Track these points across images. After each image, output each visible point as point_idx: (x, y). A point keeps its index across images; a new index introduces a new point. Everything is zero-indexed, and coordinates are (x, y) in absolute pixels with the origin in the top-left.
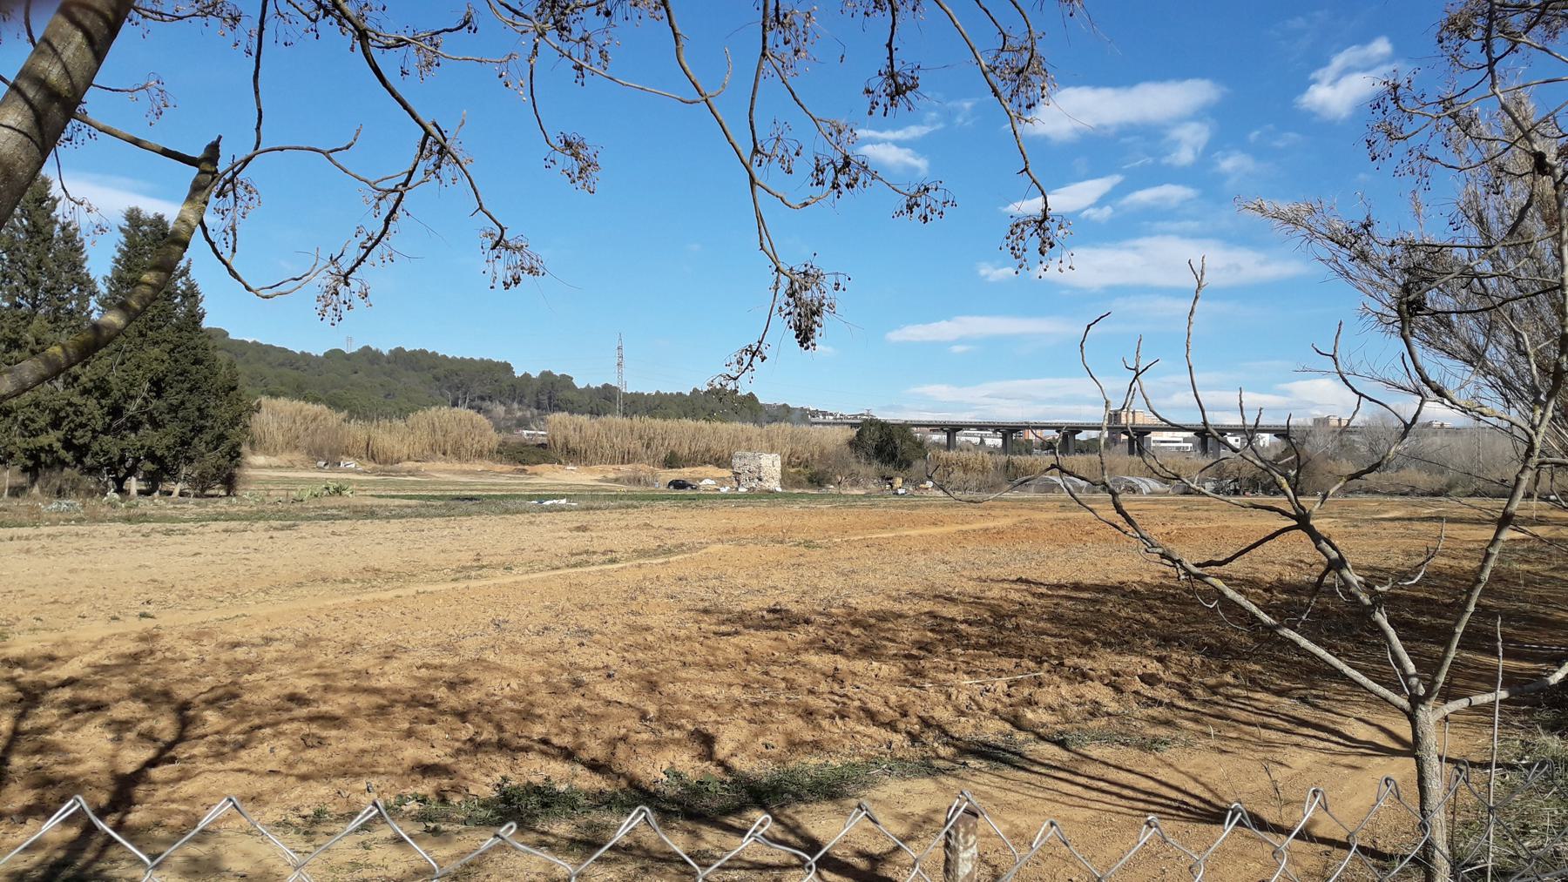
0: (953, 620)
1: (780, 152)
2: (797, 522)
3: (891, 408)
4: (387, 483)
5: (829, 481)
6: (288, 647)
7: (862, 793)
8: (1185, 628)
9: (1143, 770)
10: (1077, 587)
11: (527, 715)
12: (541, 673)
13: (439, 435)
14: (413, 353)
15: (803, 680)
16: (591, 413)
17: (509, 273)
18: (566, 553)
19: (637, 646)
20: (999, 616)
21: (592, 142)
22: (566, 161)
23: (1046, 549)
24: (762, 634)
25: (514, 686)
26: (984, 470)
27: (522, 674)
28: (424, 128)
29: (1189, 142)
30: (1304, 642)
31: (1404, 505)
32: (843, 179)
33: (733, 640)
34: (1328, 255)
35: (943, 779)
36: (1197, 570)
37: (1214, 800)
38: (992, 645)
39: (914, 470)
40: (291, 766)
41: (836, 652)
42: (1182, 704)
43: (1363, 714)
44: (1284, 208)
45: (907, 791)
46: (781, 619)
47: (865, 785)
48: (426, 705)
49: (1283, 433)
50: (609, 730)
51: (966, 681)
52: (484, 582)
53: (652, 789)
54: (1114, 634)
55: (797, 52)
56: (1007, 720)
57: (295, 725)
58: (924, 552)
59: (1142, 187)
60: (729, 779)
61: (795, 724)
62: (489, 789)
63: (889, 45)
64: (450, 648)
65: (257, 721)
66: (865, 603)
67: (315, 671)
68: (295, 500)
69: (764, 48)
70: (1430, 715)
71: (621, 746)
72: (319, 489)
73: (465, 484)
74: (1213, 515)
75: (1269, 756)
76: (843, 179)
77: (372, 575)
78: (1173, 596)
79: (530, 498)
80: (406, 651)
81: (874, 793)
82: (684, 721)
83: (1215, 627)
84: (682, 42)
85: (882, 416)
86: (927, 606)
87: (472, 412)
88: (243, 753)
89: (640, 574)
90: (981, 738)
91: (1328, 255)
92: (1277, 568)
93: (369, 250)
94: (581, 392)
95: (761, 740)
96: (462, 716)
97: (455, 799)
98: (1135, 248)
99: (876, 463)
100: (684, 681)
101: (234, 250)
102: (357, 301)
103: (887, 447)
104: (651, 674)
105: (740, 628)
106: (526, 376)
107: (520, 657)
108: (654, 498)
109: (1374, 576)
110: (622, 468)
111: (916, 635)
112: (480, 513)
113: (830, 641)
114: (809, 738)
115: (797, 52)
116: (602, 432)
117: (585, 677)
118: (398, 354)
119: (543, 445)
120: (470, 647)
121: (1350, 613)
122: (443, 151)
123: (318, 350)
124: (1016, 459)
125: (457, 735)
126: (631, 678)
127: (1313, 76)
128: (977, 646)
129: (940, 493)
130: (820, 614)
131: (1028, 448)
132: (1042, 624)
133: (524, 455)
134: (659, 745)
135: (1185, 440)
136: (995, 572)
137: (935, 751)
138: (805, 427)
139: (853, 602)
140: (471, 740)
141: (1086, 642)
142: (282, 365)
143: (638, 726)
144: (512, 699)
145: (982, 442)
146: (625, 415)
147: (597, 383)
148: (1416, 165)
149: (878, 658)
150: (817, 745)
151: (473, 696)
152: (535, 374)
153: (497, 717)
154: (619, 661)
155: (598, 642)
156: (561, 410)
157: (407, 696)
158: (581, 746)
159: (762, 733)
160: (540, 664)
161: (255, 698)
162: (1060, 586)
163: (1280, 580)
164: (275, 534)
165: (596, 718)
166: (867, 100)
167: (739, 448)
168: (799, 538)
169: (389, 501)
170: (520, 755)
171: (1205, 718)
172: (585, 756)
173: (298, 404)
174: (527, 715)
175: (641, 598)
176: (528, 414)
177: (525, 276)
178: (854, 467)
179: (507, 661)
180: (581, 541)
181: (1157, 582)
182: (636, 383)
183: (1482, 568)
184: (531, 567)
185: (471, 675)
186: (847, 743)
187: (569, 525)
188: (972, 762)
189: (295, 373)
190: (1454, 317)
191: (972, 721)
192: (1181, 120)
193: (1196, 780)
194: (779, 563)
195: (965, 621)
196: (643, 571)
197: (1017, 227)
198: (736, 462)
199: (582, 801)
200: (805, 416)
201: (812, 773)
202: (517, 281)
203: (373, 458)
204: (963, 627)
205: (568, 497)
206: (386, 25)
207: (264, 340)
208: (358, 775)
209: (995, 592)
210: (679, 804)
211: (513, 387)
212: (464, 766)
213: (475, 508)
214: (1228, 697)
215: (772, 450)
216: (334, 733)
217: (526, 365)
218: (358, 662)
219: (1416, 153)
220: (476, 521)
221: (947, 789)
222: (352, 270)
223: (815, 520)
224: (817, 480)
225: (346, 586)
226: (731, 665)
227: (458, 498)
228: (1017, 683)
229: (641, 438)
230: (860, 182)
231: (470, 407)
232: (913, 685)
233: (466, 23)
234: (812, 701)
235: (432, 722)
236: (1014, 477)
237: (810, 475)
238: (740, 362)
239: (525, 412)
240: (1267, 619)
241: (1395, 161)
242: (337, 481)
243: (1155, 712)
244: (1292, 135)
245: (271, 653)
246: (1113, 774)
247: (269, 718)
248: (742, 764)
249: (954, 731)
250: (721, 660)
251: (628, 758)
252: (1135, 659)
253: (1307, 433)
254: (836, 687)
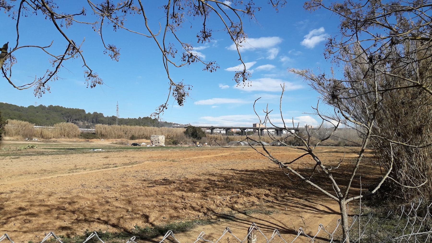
0: (214, 181)
1: (171, 52)
2: (170, 155)
3: (196, 123)
4: (47, 145)
5: (179, 143)
6: (18, 193)
7: (191, 230)
8: (275, 181)
9: (266, 220)
10: (247, 171)
11: (93, 212)
12: (96, 199)
13: (63, 131)
14: (55, 107)
15: (174, 199)
16: (109, 124)
17: (93, 83)
18: (102, 164)
19: (124, 191)
20: (227, 179)
21: (118, 47)
22: (110, 52)
23: (238, 161)
24: (161, 186)
25: (89, 203)
26: (221, 139)
27: (91, 200)
28: (69, 42)
29: (273, 53)
30: (312, 184)
31: (327, 148)
32: (191, 60)
33: (153, 188)
34: (311, 84)
35: (213, 225)
36: (285, 165)
37: (285, 227)
38: (225, 187)
39: (202, 140)
40: (21, 229)
41: (182, 191)
42: (275, 201)
43: (321, 203)
44: (300, 71)
45: (204, 229)
46: (166, 182)
47: (192, 228)
48: (62, 209)
49: (297, 130)
50: (117, 215)
51: (219, 197)
52: (77, 173)
53: (131, 231)
54: (257, 183)
55: (179, 25)
56: (230, 208)
57: (21, 217)
58: (206, 162)
59: (261, 65)
60: (153, 228)
61: (172, 211)
62: (82, 233)
63: (204, 24)
64: (69, 193)
65: (9, 216)
66: (190, 177)
67: (27, 200)
68: (19, 150)
69: (167, 23)
70: (344, 202)
71: (121, 220)
72: (26, 147)
73: (71, 145)
74: (280, 151)
75: (298, 215)
76: (191, 60)
77: (44, 172)
78: (272, 173)
79: (91, 149)
80: (55, 193)
81: (194, 230)
82: (139, 212)
83: (283, 181)
84: (147, 20)
85: (193, 125)
86: (207, 177)
87: (73, 124)
88: (5, 226)
89: (124, 170)
90: (223, 213)
91: (311, 84)
92: (297, 165)
93: (51, 76)
94: (106, 118)
95: (162, 216)
96: (74, 212)
97: (72, 237)
98: (260, 81)
99: (192, 138)
100: (139, 200)
101: (10, 76)
102: (46, 91)
103: (195, 133)
104: (129, 199)
105: (155, 185)
106: (89, 113)
107: (90, 195)
108: (128, 148)
109: (328, 167)
110: (118, 140)
111: (204, 185)
112: (75, 153)
113: (181, 188)
114: (176, 215)
115: (179, 25)
116: (112, 130)
117: (109, 200)
118: (51, 107)
119: (94, 134)
120: (74, 192)
121: (316, 177)
122: (74, 48)
123: (26, 106)
124: (229, 136)
125: (72, 218)
126: (123, 200)
127: (305, 37)
128: (221, 188)
129: (209, 146)
130: (178, 180)
131: (232, 134)
132: (238, 181)
133: (88, 136)
134: (133, 219)
135: (273, 132)
136: (225, 167)
137: (211, 217)
138: (171, 128)
139: (187, 176)
140: (76, 219)
141: (250, 186)
142: (15, 110)
143: (126, 214)
144: (88, 207)
145: (220, 132)
146: (119, 124)
147: (110, 116)
148: (336, 60)
149: (194, 192)
150: (178, 217)
151: (76, 206)
152: (92, 113)
153: (84, 212)
154: (119, 195)
155: (113, 190)
156: (100, 123)
157: (56, 207)
158: (110, 220)
159: (162, 214)
160: (96, 197)
161: (8, 209)
162: (242, 171)
163: (298, 168)
164: (13, 160)
165: (113, 212)
166: (197, 39)
167: (153, 134)
168: (170, 159)
169: (48, 150)
170: (91, 223)
171: (282, 205)
172: (111, 223)
173: (19, 122)
174: (93, 212)
175: (125, 177)
176: (90, 124)
177: (97, 85)
178: (186, 139)
179: (86, 196)
180: (106, 161)
181: (267, 169)
182: (122, 115)
183: (357, 164)
184: (91, 169)
185: (75, 200)
186: (187, 216)
187: (102, 156)
188: (221, 220)
189: (18, 112)
190: (342, 100)
191: (221, 208)
192: (271, 47)
193: (280, 222)
194: (165, 166)
195: (218, 181)
196: (125, 169)
197: (237, 75)
198: (152, 138)
199: (110, 236)
200: (170, 125)
201: (177, 225)
202: (95, 86)
203: (43, 137)
204: (217, 182)
205: (102, 149)
206: (58, 12)
207: (9, 103)
208: (42, 231)
209: (225, 173)
210: (139, 235)
211: (85, 117)
212: (75, 227)
213: (74, 152)
214: (287, 200)
215: (162, 134)
216: (34, 218)
217: (89, 110)
218: (41, 197)
219: (336, 57)
220: (74, 156)
221: (214, 228)
222: (45, 82)
223: (175, 154)
224: (175, 143)
225: (36, 175)
226: (152, 195)
227: (69, 149)
228: (232, 197)
229: (123, 131)
230: (195, 61)
231: (72, 122)
232: (204, 199)
233: (83, 12)
234: (176, 205)
235: (64, 214)
236: (228, 141)
237: (173, 141)
238: (160, 109)
239: (89, 125)
240: (303, 178)
241: (331, 59)
242: (32, 144)
243: (268, 204)
244: (300, 52)
245: (13, 195)
246: (259, 221)
247: (13, 215)
248: (157, 223)
249: (216, 211)
250: (150, 194)
251: (123, 223)
252: (263, 190)
253: (303, 130)
254: (183, 201)
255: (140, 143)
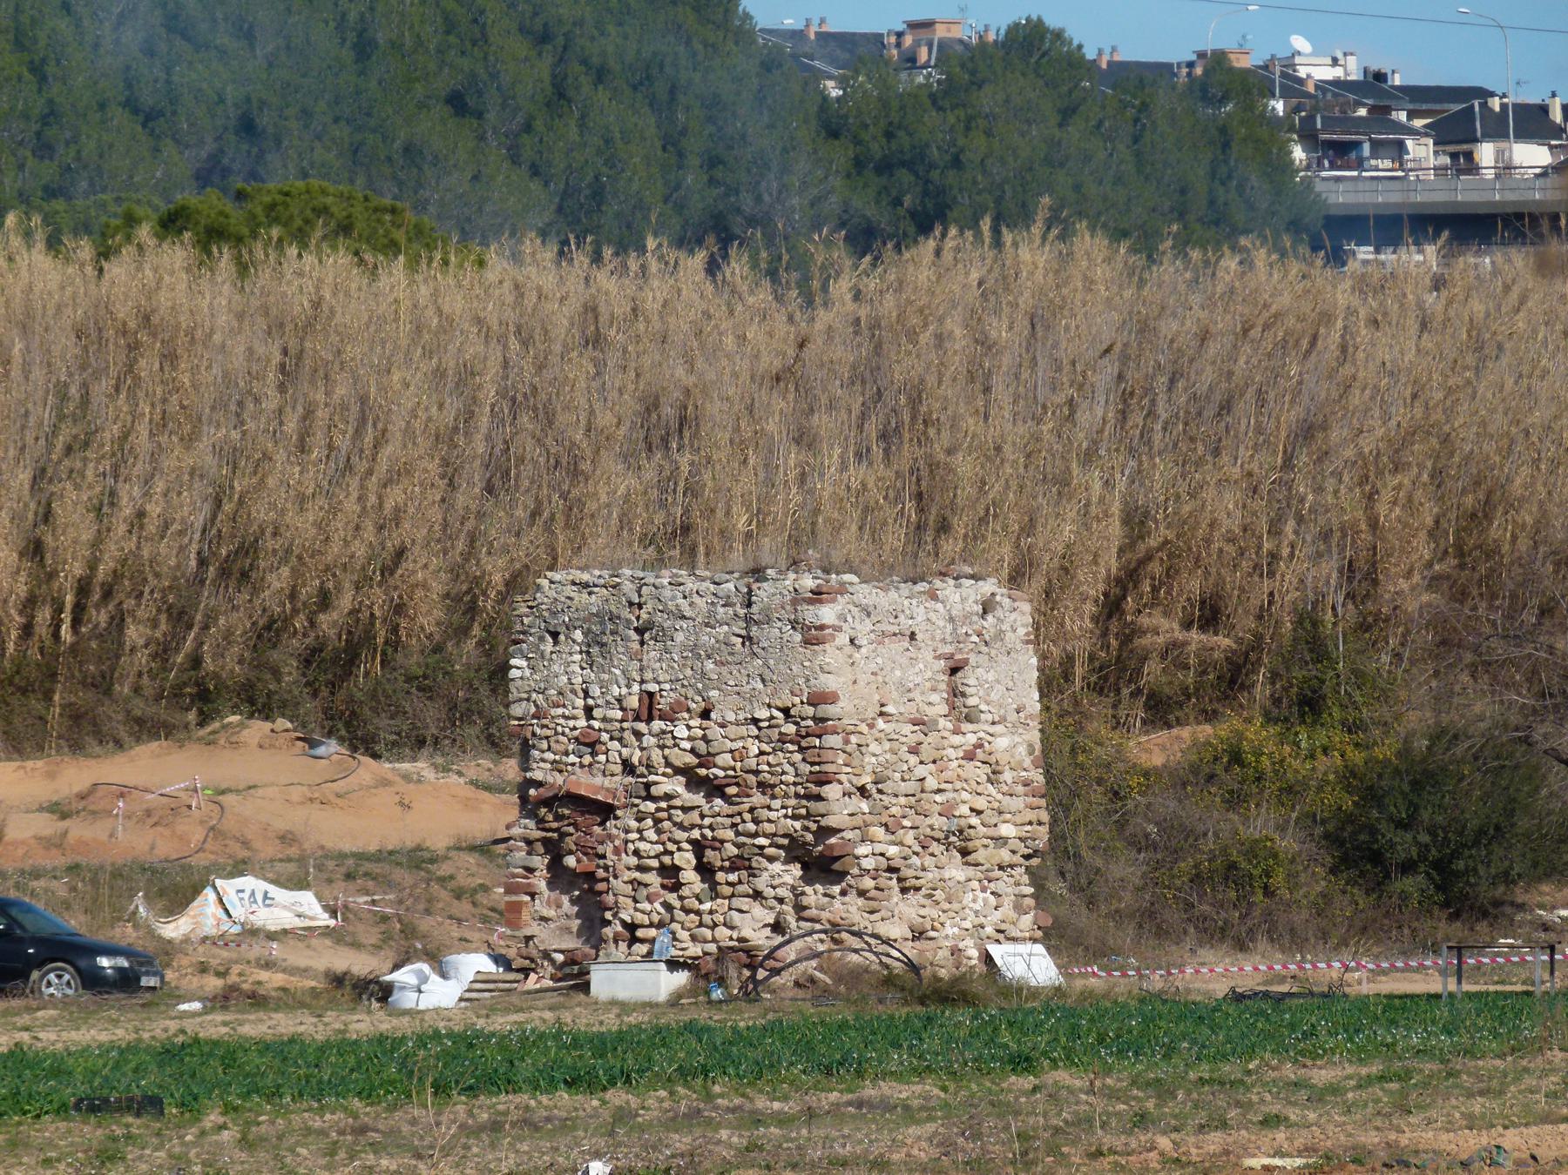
138: (1267, 277)
167: (564, 526)
198: (549, 676)
200: (1202, 153)
215: (928, 530)
255: (112, 883)
